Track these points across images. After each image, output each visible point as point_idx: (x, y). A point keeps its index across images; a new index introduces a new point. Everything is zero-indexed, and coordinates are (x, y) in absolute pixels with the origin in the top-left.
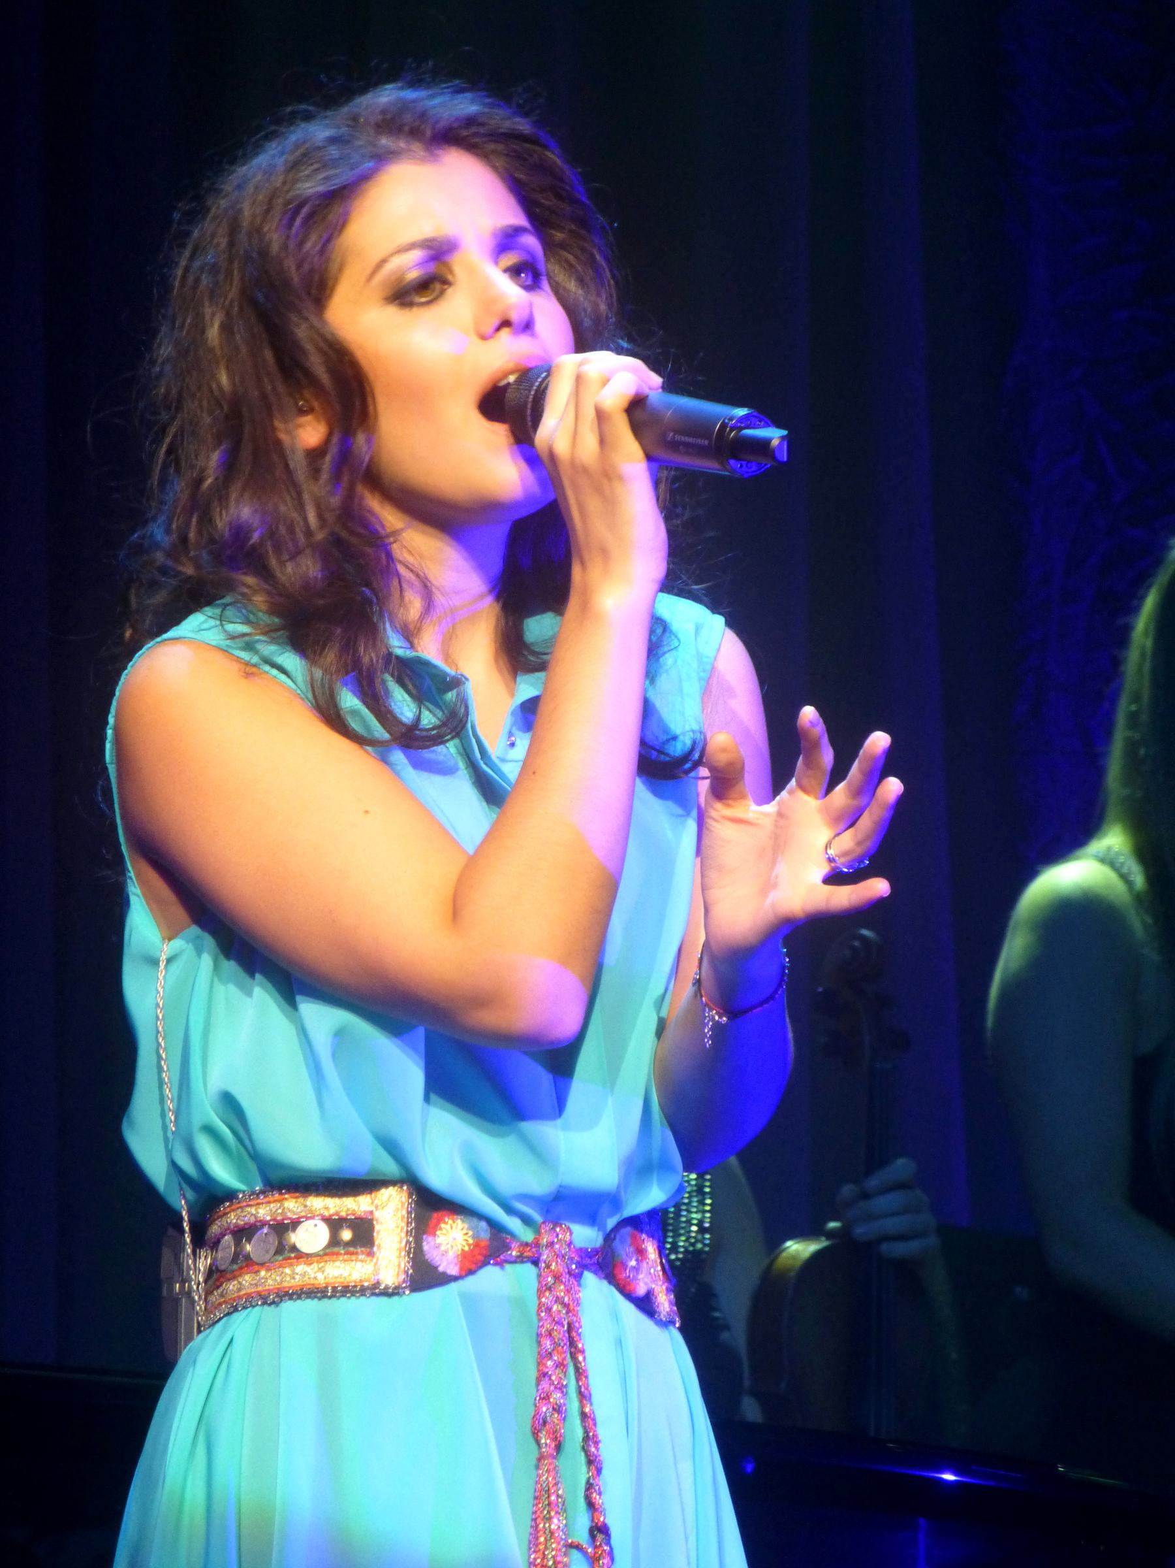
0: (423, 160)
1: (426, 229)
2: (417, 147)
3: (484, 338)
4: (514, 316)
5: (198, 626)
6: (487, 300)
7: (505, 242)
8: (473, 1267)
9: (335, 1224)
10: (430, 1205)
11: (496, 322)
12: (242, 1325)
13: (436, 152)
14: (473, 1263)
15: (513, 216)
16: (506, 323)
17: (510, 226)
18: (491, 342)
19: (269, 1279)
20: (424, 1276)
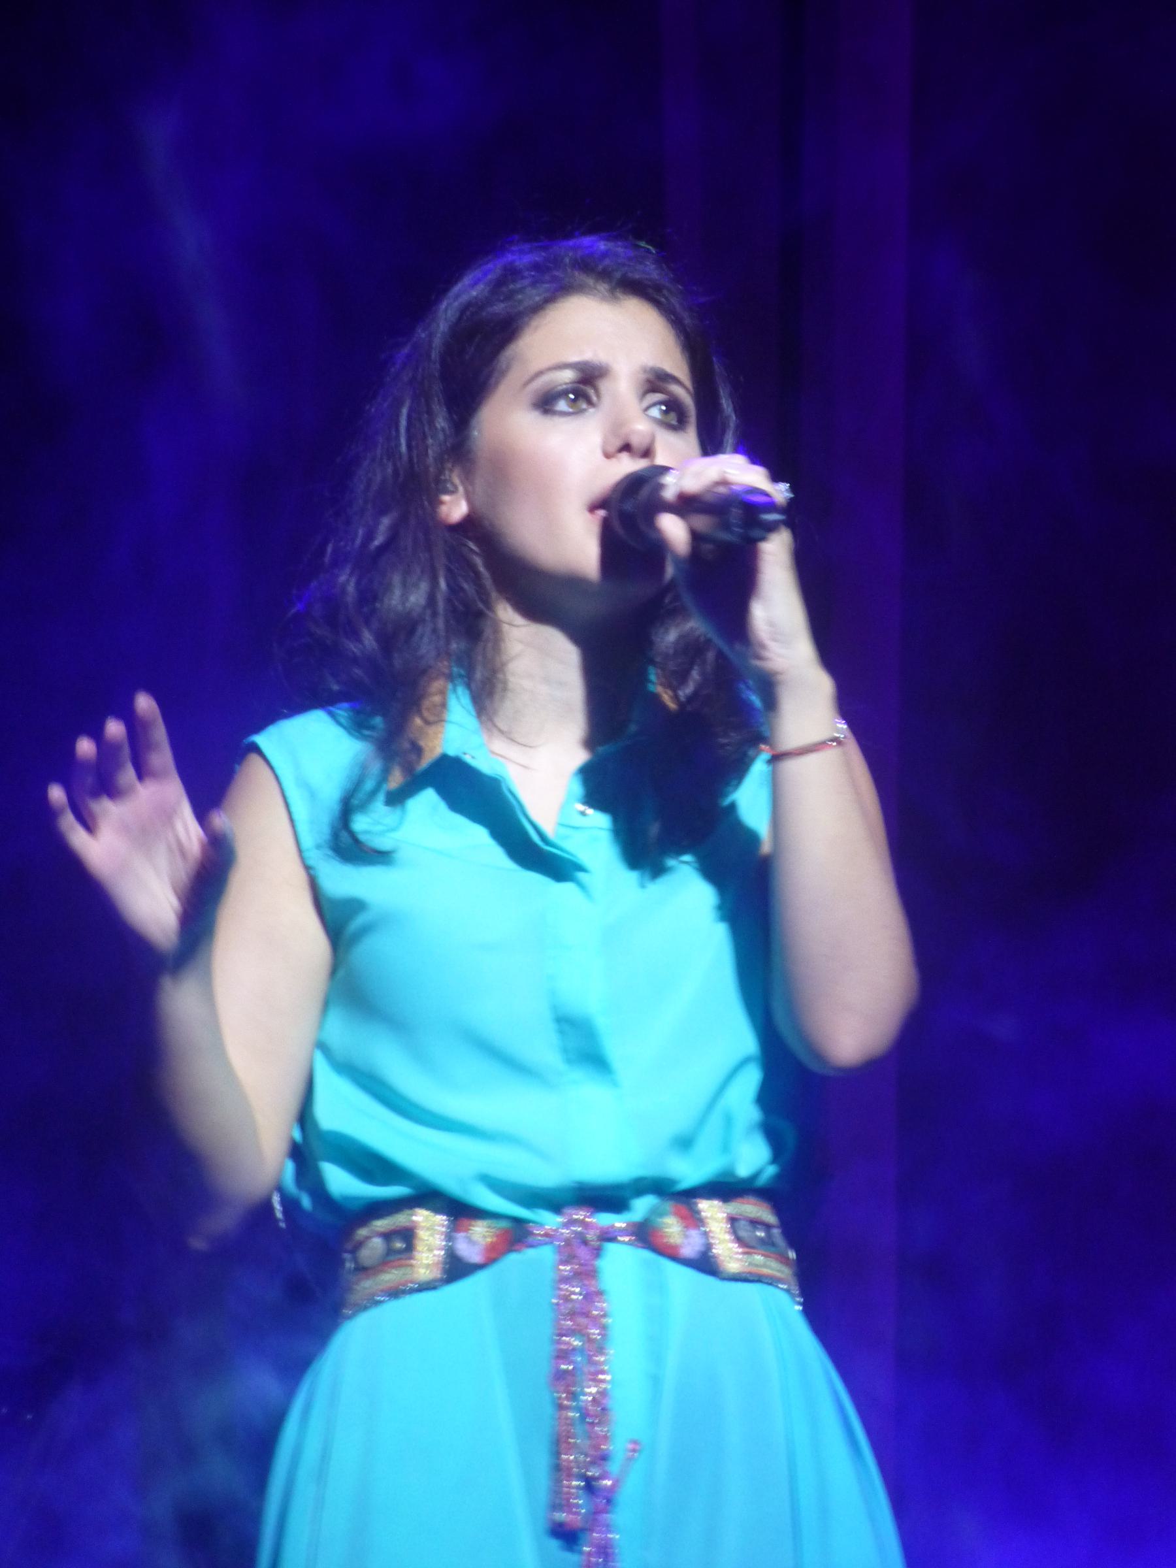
0: (603, 299)
1: (587, 354)
2: (603, 287)
3: (608, 456)
4: (636, 441)
5: (345, 705)
6: (616, 424)
7: (656, 382)
8: (493, 1255)
9: (387, 1236)
10: (460, 1212)
11: (618, 443)
12: (391, 1310)
13: (619, 294)
14: (494, 1254)
15: (675, 363)
16: (626, 448)
17: (663, 370)
18: (614, 460)
19: (390, 1277)
20: (456, 1269)
